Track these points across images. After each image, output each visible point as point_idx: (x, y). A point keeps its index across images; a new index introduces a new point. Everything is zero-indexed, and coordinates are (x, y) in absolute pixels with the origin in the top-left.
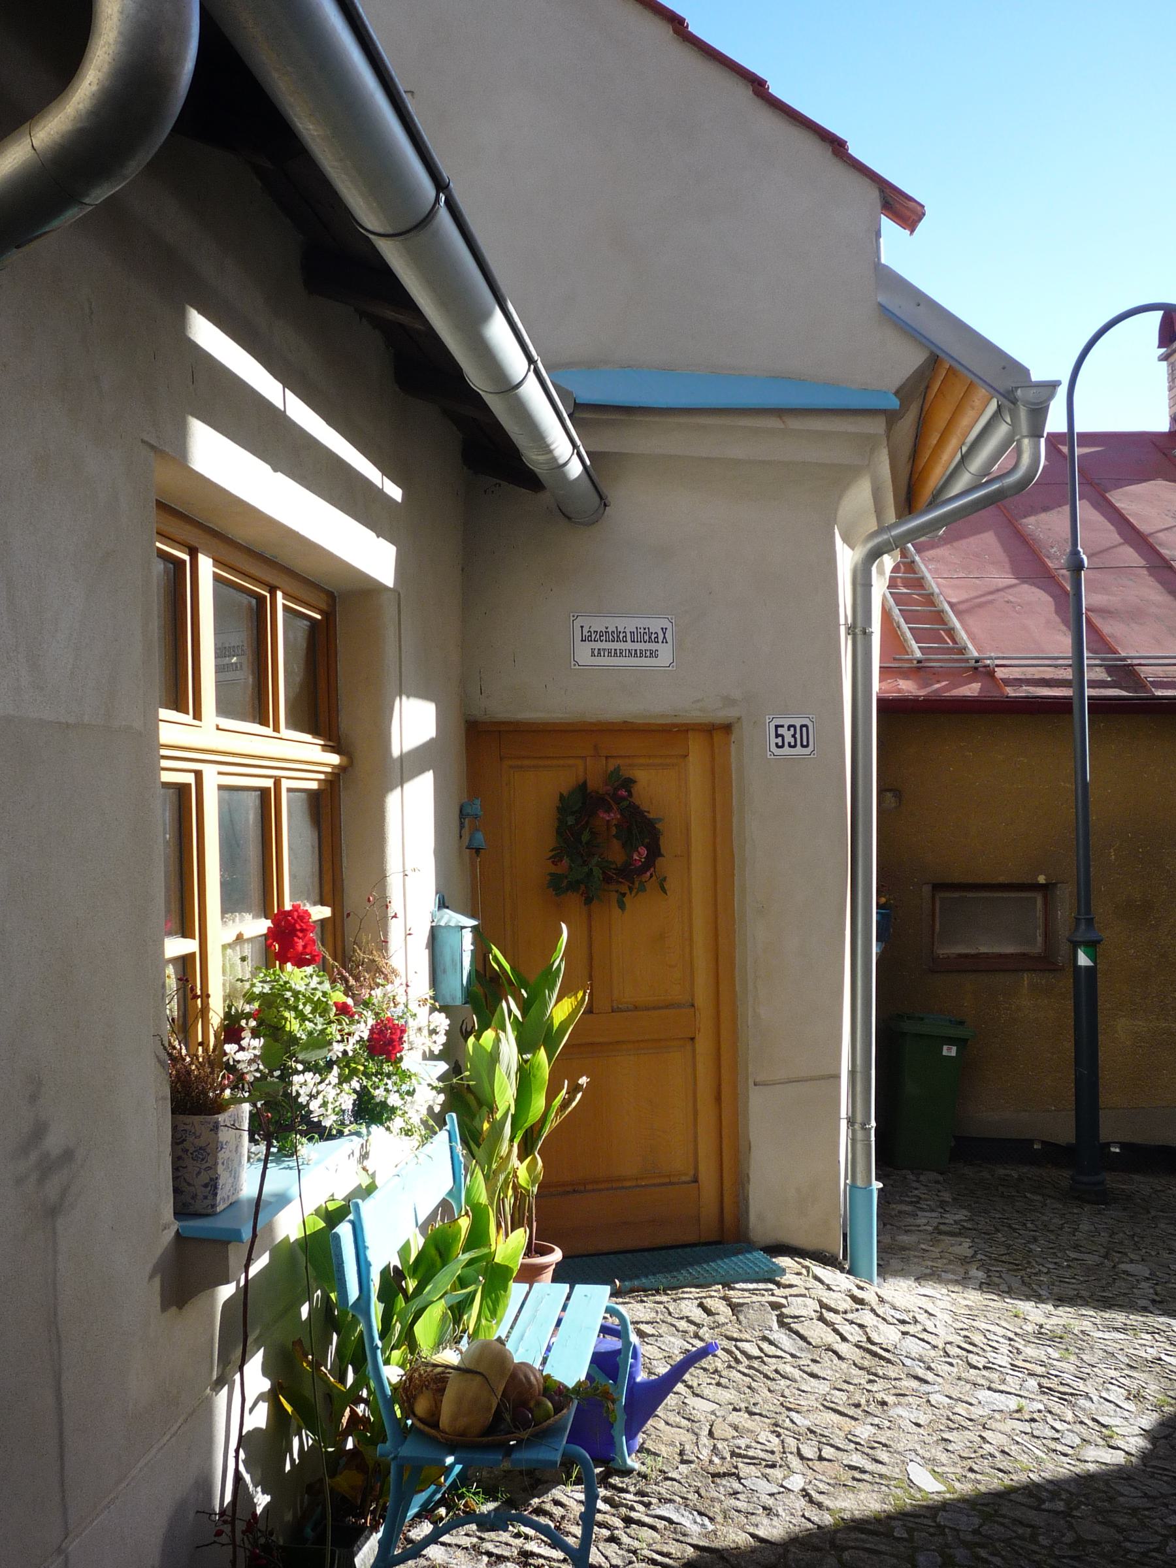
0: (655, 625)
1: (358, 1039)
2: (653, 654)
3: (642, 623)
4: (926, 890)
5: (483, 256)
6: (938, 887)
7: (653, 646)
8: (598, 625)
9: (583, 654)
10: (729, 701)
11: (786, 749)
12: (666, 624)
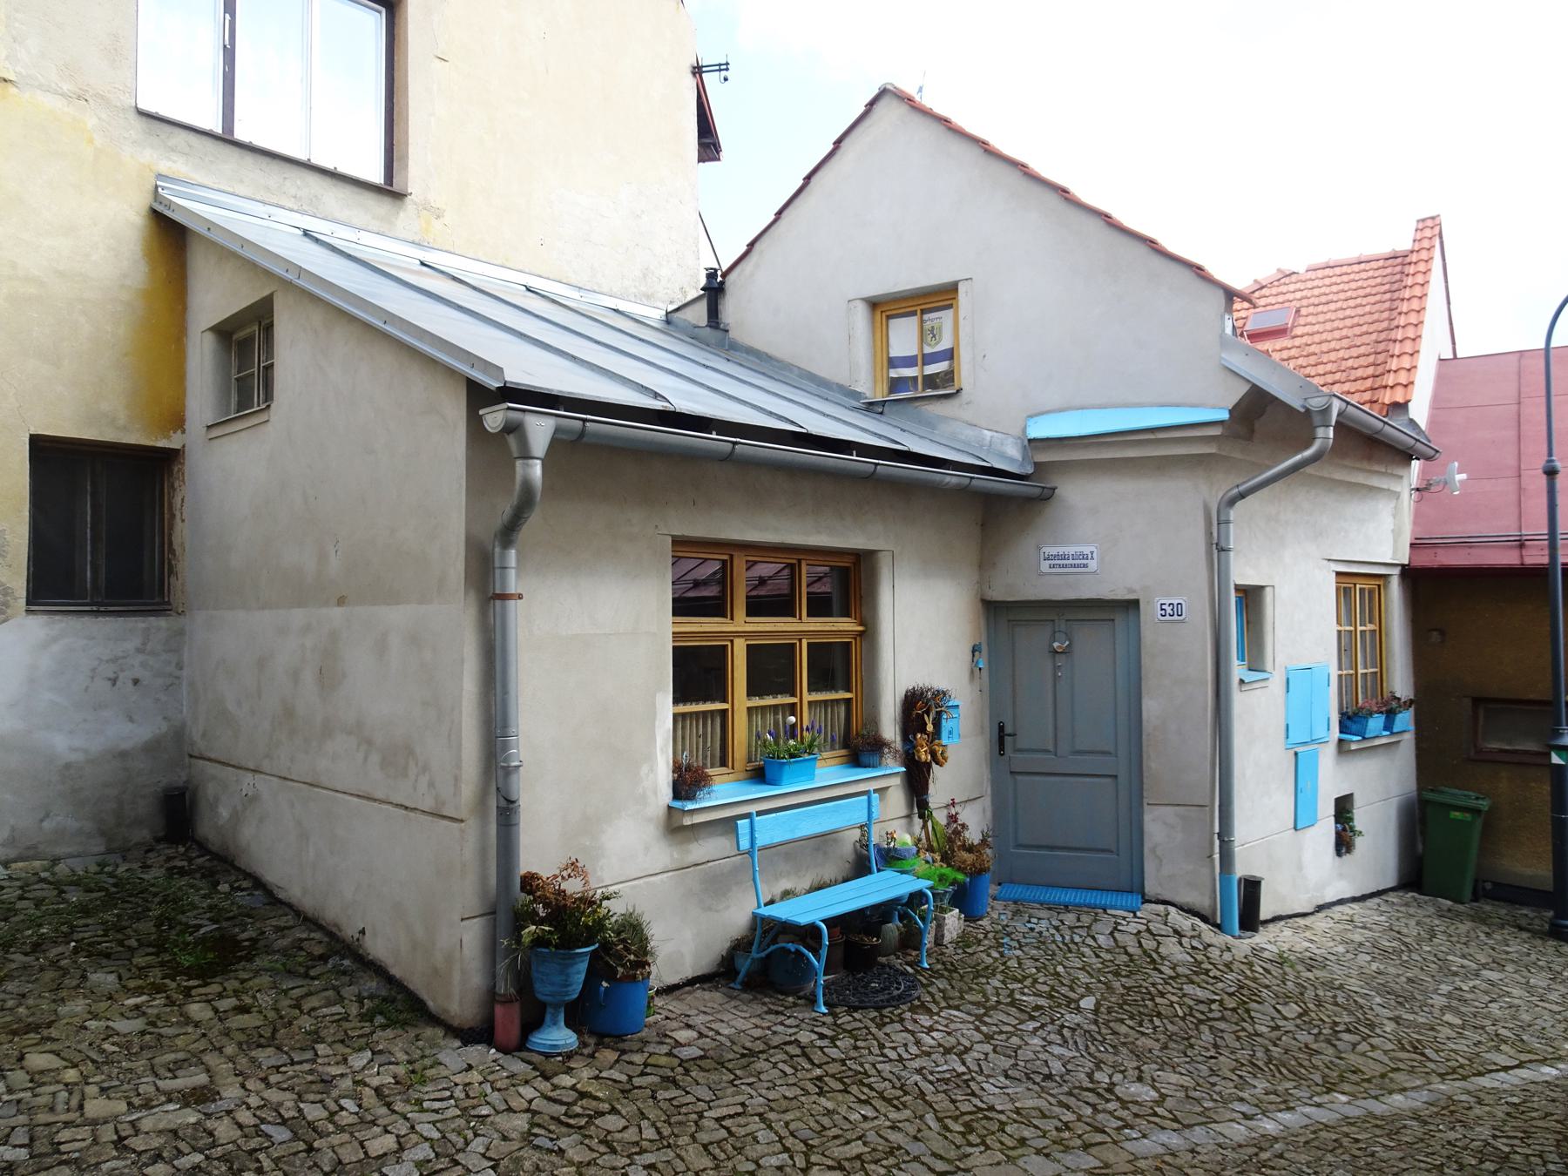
0: (1086, 550)
1: (350, 1019)
2: (1085, 566)
3: (1079, 549)
4: (1467, 702)
5: (918, 289)
6: (1477, 701)
7: (1085, 562)
8: (1053, 551)
9: (1045, 567)
10: (1131, 591)
11: (1168, 618)
12: (1093, 549)
